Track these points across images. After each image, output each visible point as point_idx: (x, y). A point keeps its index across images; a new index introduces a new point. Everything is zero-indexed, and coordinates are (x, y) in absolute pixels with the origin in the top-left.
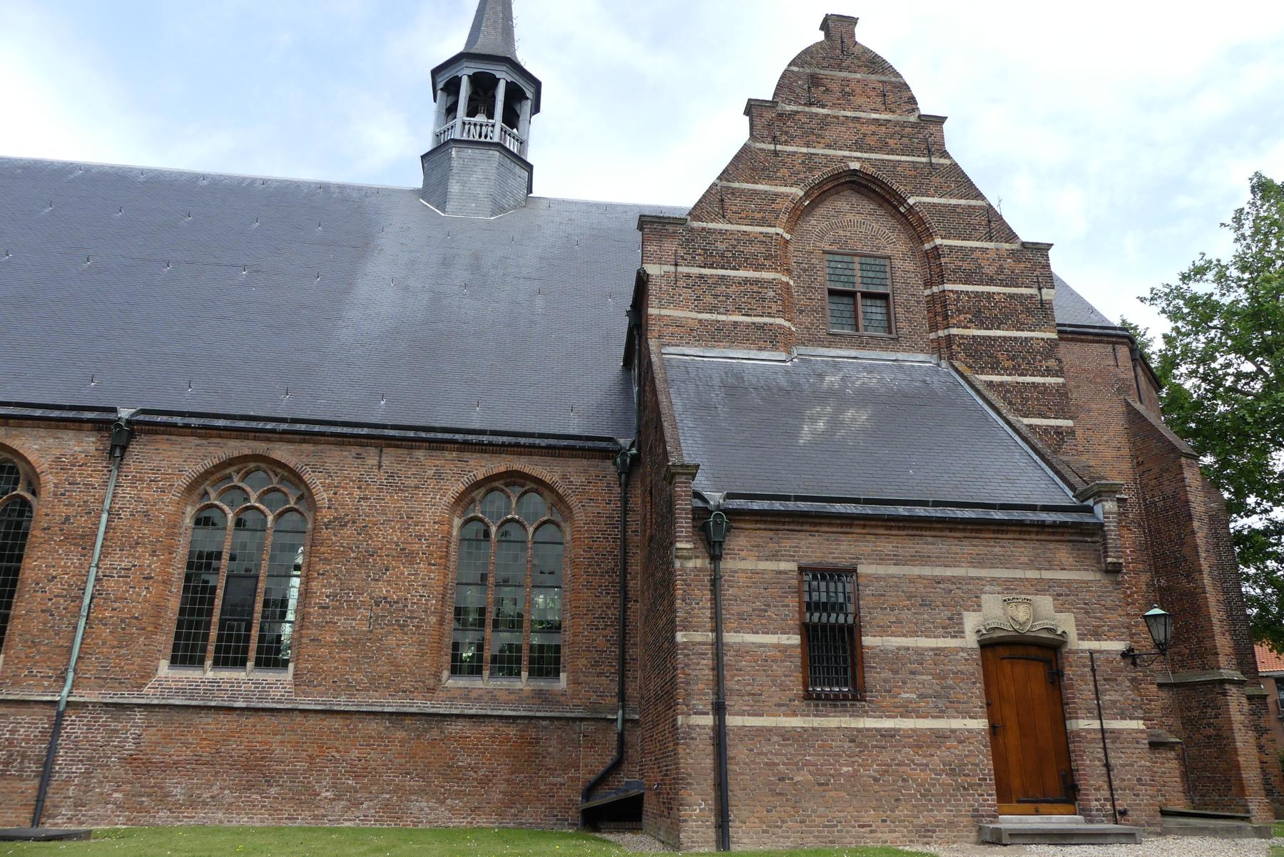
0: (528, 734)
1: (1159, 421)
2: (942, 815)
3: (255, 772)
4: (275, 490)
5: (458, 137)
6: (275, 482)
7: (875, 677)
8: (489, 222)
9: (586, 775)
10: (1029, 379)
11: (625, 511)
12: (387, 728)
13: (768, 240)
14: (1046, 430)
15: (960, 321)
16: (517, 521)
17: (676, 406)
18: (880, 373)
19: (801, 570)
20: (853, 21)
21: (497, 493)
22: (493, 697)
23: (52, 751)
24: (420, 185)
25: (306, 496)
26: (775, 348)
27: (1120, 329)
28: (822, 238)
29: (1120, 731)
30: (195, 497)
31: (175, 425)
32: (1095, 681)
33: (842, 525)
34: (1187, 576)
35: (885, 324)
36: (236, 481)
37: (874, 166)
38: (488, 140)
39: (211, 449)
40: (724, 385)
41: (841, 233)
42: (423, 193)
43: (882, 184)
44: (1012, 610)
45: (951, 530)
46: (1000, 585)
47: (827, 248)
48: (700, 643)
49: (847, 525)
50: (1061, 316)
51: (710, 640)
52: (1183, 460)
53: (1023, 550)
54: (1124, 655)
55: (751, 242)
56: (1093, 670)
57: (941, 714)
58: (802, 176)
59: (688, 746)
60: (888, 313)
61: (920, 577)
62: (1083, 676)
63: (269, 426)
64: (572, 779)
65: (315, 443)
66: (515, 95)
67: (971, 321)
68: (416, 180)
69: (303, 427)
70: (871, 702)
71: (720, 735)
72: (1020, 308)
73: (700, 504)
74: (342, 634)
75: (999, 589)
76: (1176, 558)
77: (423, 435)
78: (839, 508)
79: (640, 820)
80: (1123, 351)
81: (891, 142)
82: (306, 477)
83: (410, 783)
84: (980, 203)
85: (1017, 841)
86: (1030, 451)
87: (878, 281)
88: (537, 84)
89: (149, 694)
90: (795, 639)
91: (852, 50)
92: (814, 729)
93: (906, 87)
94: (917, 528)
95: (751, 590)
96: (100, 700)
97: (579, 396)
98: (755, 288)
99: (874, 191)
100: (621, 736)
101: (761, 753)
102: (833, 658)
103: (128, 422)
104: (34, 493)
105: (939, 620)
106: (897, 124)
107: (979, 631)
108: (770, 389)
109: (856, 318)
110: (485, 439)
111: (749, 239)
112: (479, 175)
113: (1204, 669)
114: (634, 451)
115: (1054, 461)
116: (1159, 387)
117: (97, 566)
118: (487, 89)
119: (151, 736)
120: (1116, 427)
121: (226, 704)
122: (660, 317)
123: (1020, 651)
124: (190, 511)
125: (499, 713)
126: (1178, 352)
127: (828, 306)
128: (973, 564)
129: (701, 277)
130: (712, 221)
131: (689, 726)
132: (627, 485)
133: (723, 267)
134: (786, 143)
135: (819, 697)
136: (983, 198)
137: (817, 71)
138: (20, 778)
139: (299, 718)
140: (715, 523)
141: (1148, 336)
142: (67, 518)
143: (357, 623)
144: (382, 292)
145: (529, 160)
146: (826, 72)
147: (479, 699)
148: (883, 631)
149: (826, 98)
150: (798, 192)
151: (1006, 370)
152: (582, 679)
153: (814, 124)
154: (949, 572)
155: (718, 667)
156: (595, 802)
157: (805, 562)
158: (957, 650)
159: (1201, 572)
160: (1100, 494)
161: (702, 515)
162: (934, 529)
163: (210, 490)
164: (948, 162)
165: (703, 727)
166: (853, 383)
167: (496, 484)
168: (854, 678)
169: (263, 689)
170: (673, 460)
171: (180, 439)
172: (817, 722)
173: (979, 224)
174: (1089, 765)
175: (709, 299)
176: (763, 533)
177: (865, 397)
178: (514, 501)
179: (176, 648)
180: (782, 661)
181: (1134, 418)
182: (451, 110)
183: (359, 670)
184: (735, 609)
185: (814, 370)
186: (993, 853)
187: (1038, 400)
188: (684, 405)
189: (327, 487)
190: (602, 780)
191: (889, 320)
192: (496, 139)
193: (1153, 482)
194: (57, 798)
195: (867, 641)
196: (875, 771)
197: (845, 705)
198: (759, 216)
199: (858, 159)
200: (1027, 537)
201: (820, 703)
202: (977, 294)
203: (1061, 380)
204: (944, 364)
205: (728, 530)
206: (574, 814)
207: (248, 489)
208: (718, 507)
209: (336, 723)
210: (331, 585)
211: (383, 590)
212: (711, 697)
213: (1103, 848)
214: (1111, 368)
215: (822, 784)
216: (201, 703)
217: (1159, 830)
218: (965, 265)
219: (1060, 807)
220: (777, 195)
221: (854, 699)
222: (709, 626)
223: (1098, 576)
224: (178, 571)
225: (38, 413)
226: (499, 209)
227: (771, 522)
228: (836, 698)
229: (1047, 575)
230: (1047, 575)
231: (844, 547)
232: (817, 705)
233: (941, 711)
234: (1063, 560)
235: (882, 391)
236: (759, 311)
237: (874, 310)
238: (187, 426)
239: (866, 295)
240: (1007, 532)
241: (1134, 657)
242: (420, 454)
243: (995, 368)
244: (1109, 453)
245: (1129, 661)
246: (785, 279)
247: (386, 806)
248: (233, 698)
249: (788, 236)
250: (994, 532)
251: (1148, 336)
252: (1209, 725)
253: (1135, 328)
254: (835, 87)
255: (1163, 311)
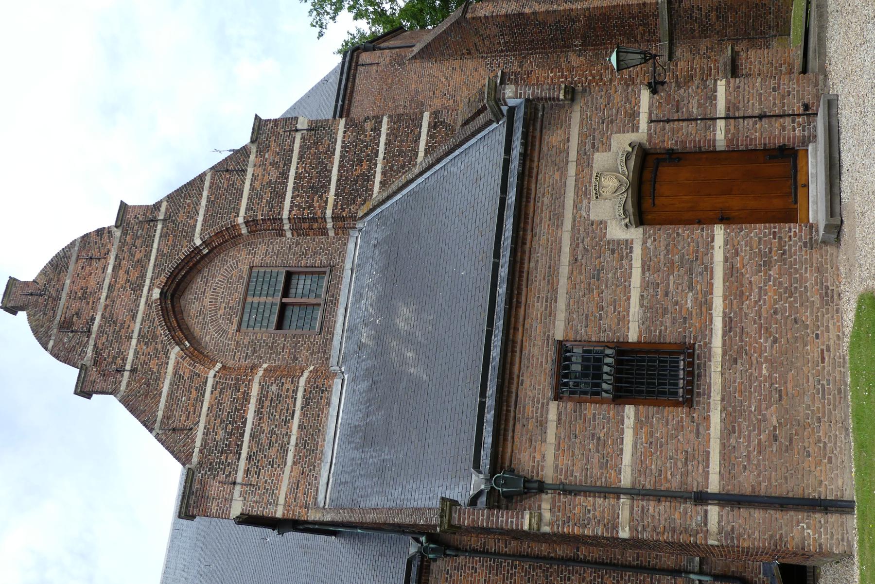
1: (432, 31)
2: (811, 278)
7: (670, 332)
10: (382, 148)
11: (485, 552)
13: (219, 387)
14: (431, 136)
15: (320, 207)
18: (363, 287)
19: (557, 397)
20: (12, 282)
26: (329, 389)
27: (344, 58)
28: (224, 331)
29: (728, 102)
32: (678, 120)
33: (513, 352)
34: (574, 22)
40: (361, 447)
41: (221, 312)
45: (524, 243)
46: (581, 202)
47: (235, 327)
48: (631, 513)
49: (514, 347)
51: (628, 502)
52: (469, 16)
53: (547, 176)
54: (654, 91)
55: (219, 404)
56: (668, 121)
57: (708, 269)
58: (159, 347)
59: (740, 535)
61: (569, 278)
67: (321, 197)
70: (695, 338)
71: (730, 500)
72: (313, 150)
73: (483, 499)
75: (585, 202)
76: (557, 29)
78: (495, 353)
79: (804, 568)
80: (365, 57)
81: (138, 256)
84: (208, 178)
85: (837, 210)
87: (273, 280)
90: (630, 410)
91: (41, 286)
92: (723, 400)
93: (85, 238)
94: (521, 276)
95: (576, 452)
98: (267, 403)
99: (184, 276)
101: (748, 457)
102: (652, 374)
106: (121, 249)
107: (626, 225)
108: (369, 400)
109: (307, 305)
111: (218, 403)
113: (657, 16)
114: (423, 539)
115: (462, 137)
116: (401, 28)
120: (434, 70)
122: (287, 505)
126: (371, 9)
127: (293, 331)
129: (249, 458)
130: (194, 442)
131: (720, 533)
132: (457, 549)
133: (242, 435)
134: (124, 360)
137: (56, 322)
140: (505, 485)
146: (59, 313)
148: (623, 319)
149: (85, 317)
150: (175, 352)
151: (370, 168)
153: (109, 330)
158: (645, 249)
159: (570, 10)
160: (498, 101)
162: (522, 259)
164: (164, 204)
165: (721, 517)
166: (370, 316)
170: (435, 520)
172: (716, 396)
175: (273, 452)
177: (385, 305)
180: (652, 426)
181: (426, 53)
184: (596, 471)
188: (378, 493)
191: (312, 273)
193: (487, 43)
195: (633, 336)
196: (766, 341)
197: (699, 366)
199: (150, 289)
200: (535, 171)
201: (696, 390)
202: (295, 189)
203: (385, 119)
204: (359, 225)
205: (512, 471)
208: (488, 481)
212: (689, 506)
213: (843, 130)
214: (380, 69)
217: (821, 77)
218: (267, 197)
219: (800, 164)
220: (175, 373)
221: (692, 355)
222: (613, 501)
223: (577, 107)
227: (507, 424)
228: (691, 374)
229: (573, 155)
230: (573, 155)
231: (536, 351)
233: (706, 269)
234: (559, 139)
235: (380, 288)
236: (290, 401)
237: (301, 286)
240: (529, 189)
243: (368, 178)
244: (457, 77)
246: (261, 372)
249: (219, 366)
250: (528, 201)
251: (355, 32)
252: (707, 16)
253: (347, 43)
254: (76, 305)
255: (333, 18)
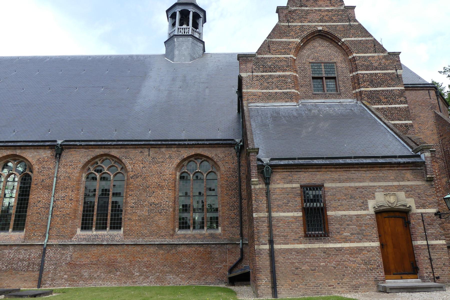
0: (206, 249)
2: (362, 281)
3: (111, 267)
4: (113, 166)
5: (176, 33)
6: (113, 163)
7: (333, 227)
8: (189, 64)
9: (230, 264)
11: (240, 166)
12: (157, 250)
14: (401, 125)
16: (200, 172)
17: (253, 125)
18: (333, 107)
19: (301, 186)
21: (192, 162)
22: (194, 237)
23: (43, 261)
24: (164, 52)
25: (124, 168)
26: (292, 101)
27: (431, 84)
30: (85, 170)
31: (76, 145)
32: (424, 225)
33: (317, 168)
35: (335, 88)
36: (99, 164)
37: (328, 28)
38: (188, 34)
39: (90, 153)
40: (272, 116)
41: (316, 55)
42: (166, 55)
43: (331, 34)
44: (388, 198)
45: (361, 168)
47: (311, 61)
48: (262, 217)
49: (319, 168)
50: (406, 81)
53: (391, 173)
54: (436, 214)
56: (423, 221)
57: (360, 241)
58: (299, 34)
60: (336, 85)
62: (418, 223)
63: (109, 143)
64: (224, 266)
65: (126, 148)
66: (196, 16)
67: (369, 85)
68: (163, 51)
69: (121, 143)
70: (332, 237)
72: (388, 78)
74: (139, 216)
77: (164, 143)
78: (316, 162)
79: (249, 281)
80: (433, 93)
81: (334, 18)
82: (123, 161)
83: (167, 269)
84: (370, 38)
85: (393, 291)
86: (394, 134)
87: (331, 72)
88: (204, 12)
89: (74, 241)
90: (300, 214)
92: (309, 249)
94: (348, 168)
96: (58, 243)
97: (222, 126)
98: (283, 79)
99: (328, 37)
100: (242, 249)
101: (288, 259)
102: (316, 221)
103: (61, 145)
104: (32, 172)
105: (352, 205)
106: (336, 11)
107: (374, 207)
108: (290, 117)
109: (323, 87)
110: (186, 143)
111: (280, 60)
112: (185, 47)
114: (241, 144)
117: (54, 196)
118: (187, 17)
119: (75, 255)
120: (431, 122)
121: (100, 243)
123: (392, 214)
124: (84, 175)
125: (196, 243)
128: (371, 181)
129: (262, 76)
131: (259, 249)
132: (239, 156)
133: (270, 72)
134: (293, 22)
135: (310, 236)
136: (372, 36)
138: (33, 271)
139: (126, 247)
141: (443, 86)
142: (43, 180)
143: (144, 212)
144: (151, 91)
145: (203, 40)
147: (189, 238)
148: (336, 209)
151: (384, 103)
152: (227, 229)
154: (361, 184)
155: (270, 226)
156: (233, 275)
157: (303, 183)
158: (366, 215)
160: (423, 150)
161: (261, 168)
162: (355, 168)
163: (90, 167)
164: (357, 23)
165: (265, 250)
167: (192, 159)
168: (324, 228)
169: (113, 237)
170: (250, 147)
171: (79, 150)
173: (371, 47)
174: (422, 260)
175: (266, 84)
176: (286, 173)
178: (198, 165)
179: (82, 224)
182: (174, 25)
183: (146, 229)
184: (276, 203)
185: (307, 108)
186: (381, 298)
187: (397, 113)
188: (256, 125)
189: (131, 164)
190: (236, 266)
191: (336, 87)
192: (190, 33)
193: (447, 143)
194: (46, 278)
195: (329, 213)
196: (334, 264)
198: (284, 51)
200: (393, 169)
201: (311, 238)
203: (406, 105)
204: (359, 102)
205: (272, 172)
206: (226, 279)
207: (104, 166)
208: (267, 164)
209: (139, 248)
210: (134, 199)
211: (153, 200)
212: (268, 238)
213: (430, 293)
214: (428, 100)
215: (313, 270)
216: (92, 243)
218: (366, 63)
220: (290, 42)
221: (325, 236)
223: (424, 183)
224: (81, 197)
225: (31, 144)
226: (193, 59)
229: (402, 183)
230: (402, 183)
231: (318, 177)
232: (310, 239)
233: (360, 240)
234: (409, 177)
235: (334, 114)
236: (285, 87)
238: (81, 145)
239: (327, 78)
240: (385, 167)
241: (440, 215)
242: (163, 150)
244: (428, 133)
245: (438, 216)
246: (295, 74)
247: (158, 277)
248: (102, 241)
249: (295, 58)
250: (379, 167)
251: (443, 86)
